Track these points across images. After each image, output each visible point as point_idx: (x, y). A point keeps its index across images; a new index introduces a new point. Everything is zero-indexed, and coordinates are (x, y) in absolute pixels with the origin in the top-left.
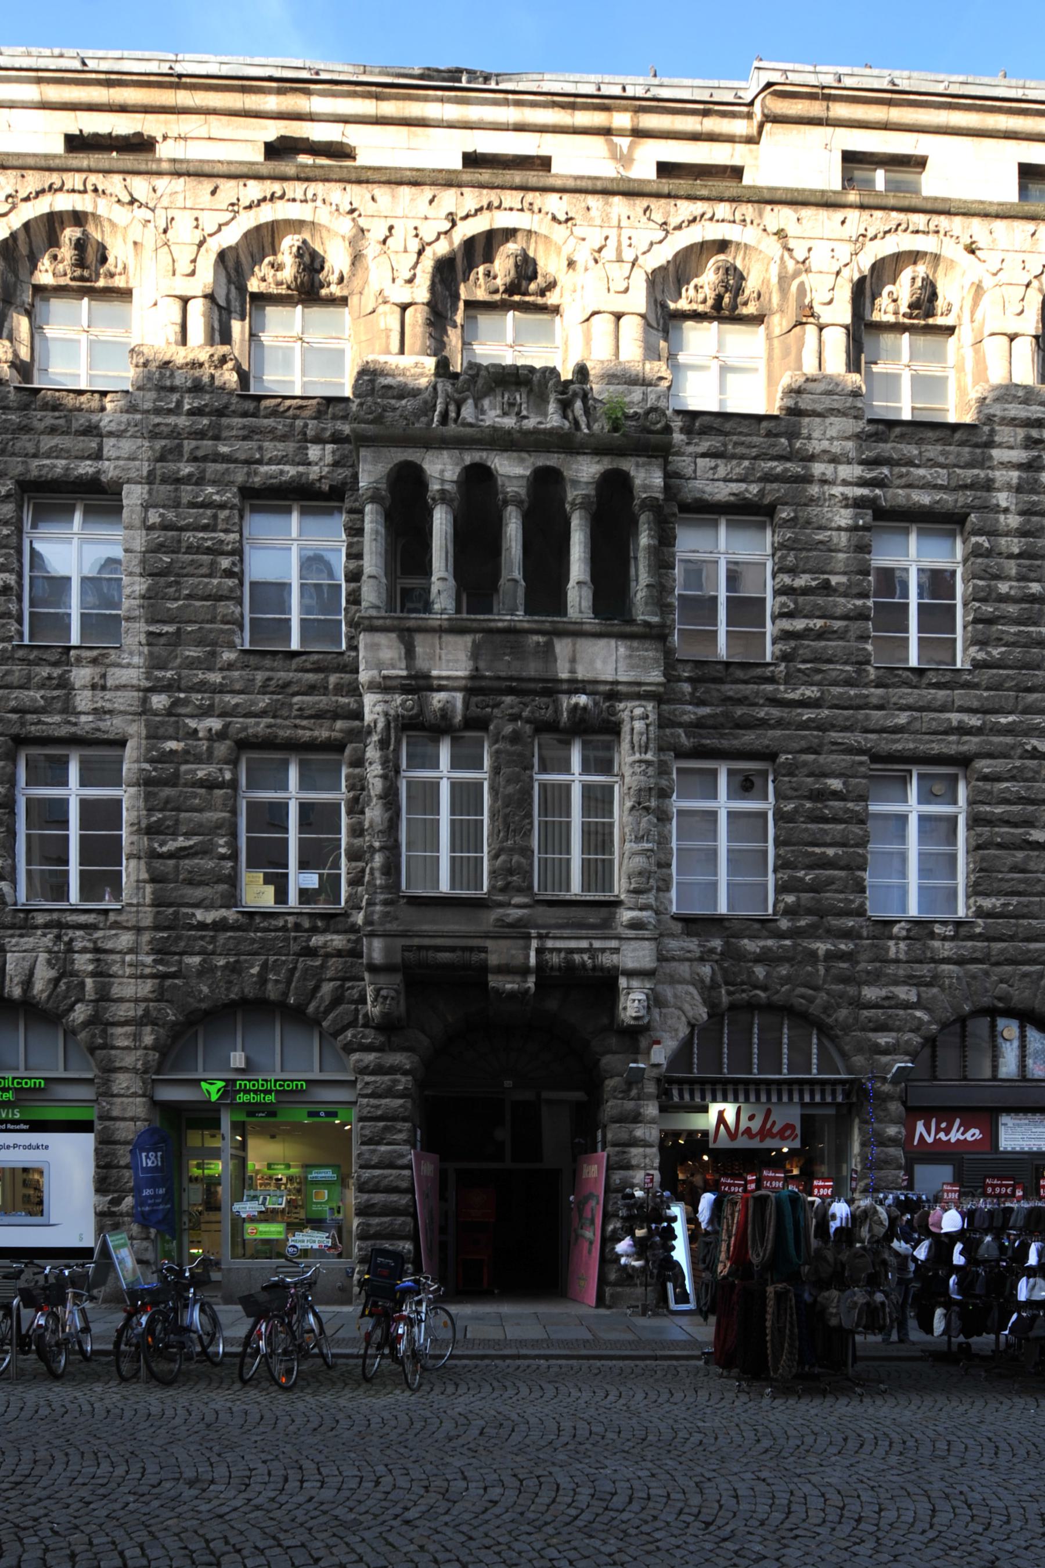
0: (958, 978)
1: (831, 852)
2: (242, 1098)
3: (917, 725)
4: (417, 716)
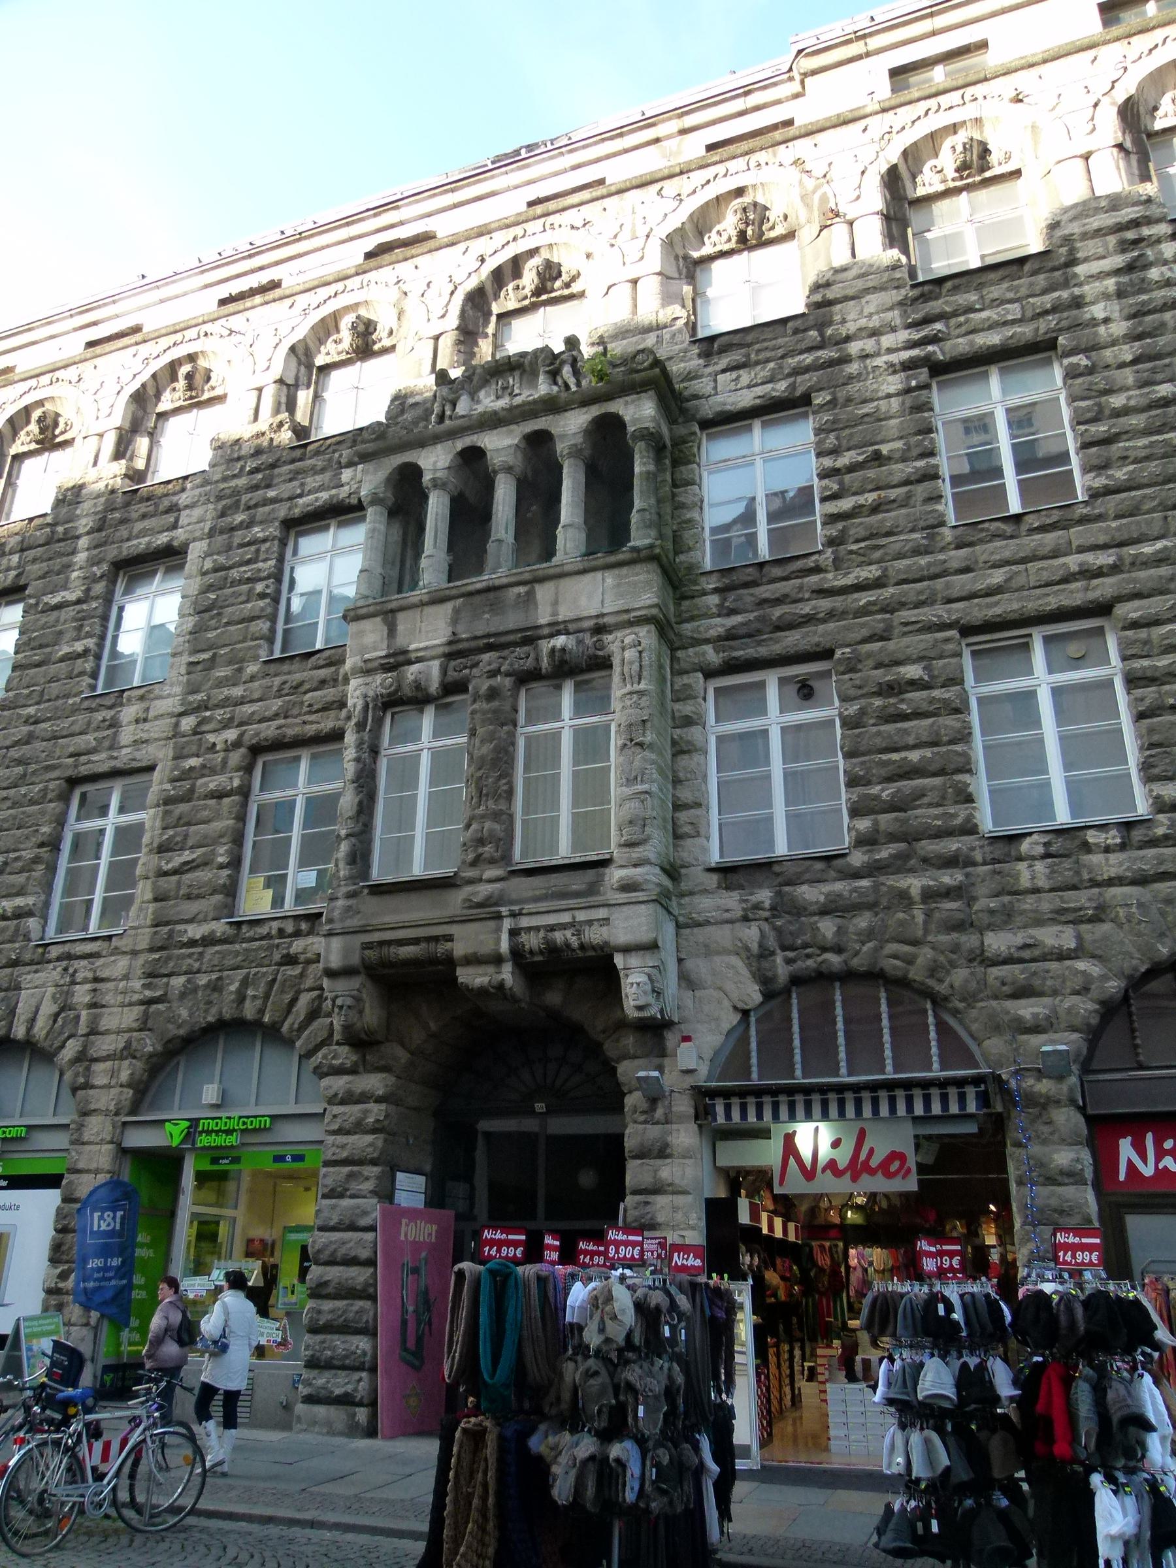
0: (1140, 905)
1: (914, 756)
2: (203, 1141)
3: (1021, 580)
4: (396, 691)
